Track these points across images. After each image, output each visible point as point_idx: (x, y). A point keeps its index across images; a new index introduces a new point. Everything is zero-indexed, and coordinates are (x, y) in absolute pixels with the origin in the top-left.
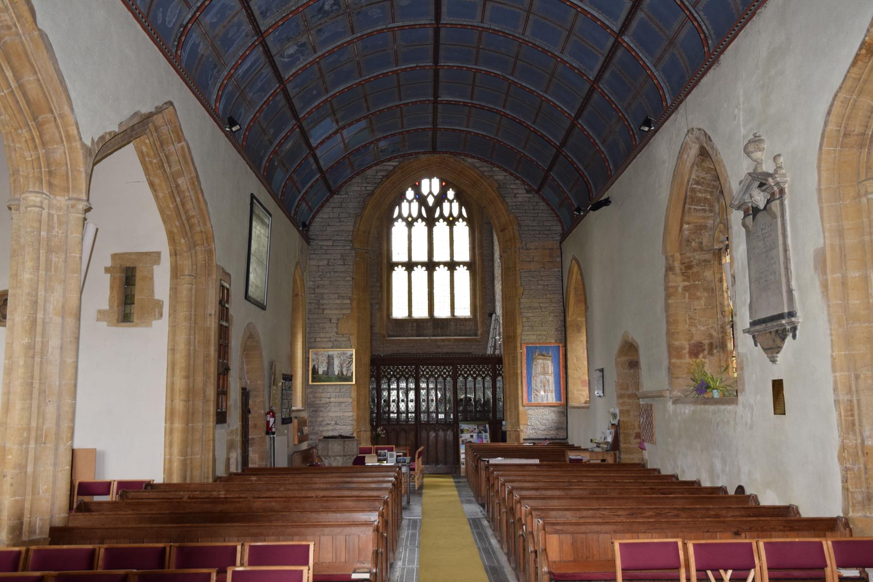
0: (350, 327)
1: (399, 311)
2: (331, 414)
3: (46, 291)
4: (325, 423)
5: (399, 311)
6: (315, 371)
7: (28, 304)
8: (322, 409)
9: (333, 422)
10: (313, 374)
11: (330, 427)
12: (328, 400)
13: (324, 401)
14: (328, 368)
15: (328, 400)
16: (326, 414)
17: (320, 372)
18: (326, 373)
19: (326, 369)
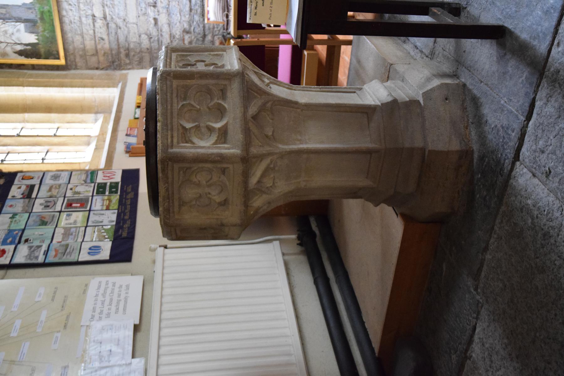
0: (409, 16)
1: (248, 22)
2: (132, 17)
3: (178, 118)
4: (154, 33)
5: (248, 22)
6: (30, 52)
7: (173, 16)
8: (122, 39)
9: (151, 12)
10: (38, 56)
11: (163, 19)
12: (99, 23)
13: (101, 31)
14: (19, 20)
15: (99, 23)
16: (133, 29)
17: (32, 39)
18: (31, 25)
19: (21, 26)
